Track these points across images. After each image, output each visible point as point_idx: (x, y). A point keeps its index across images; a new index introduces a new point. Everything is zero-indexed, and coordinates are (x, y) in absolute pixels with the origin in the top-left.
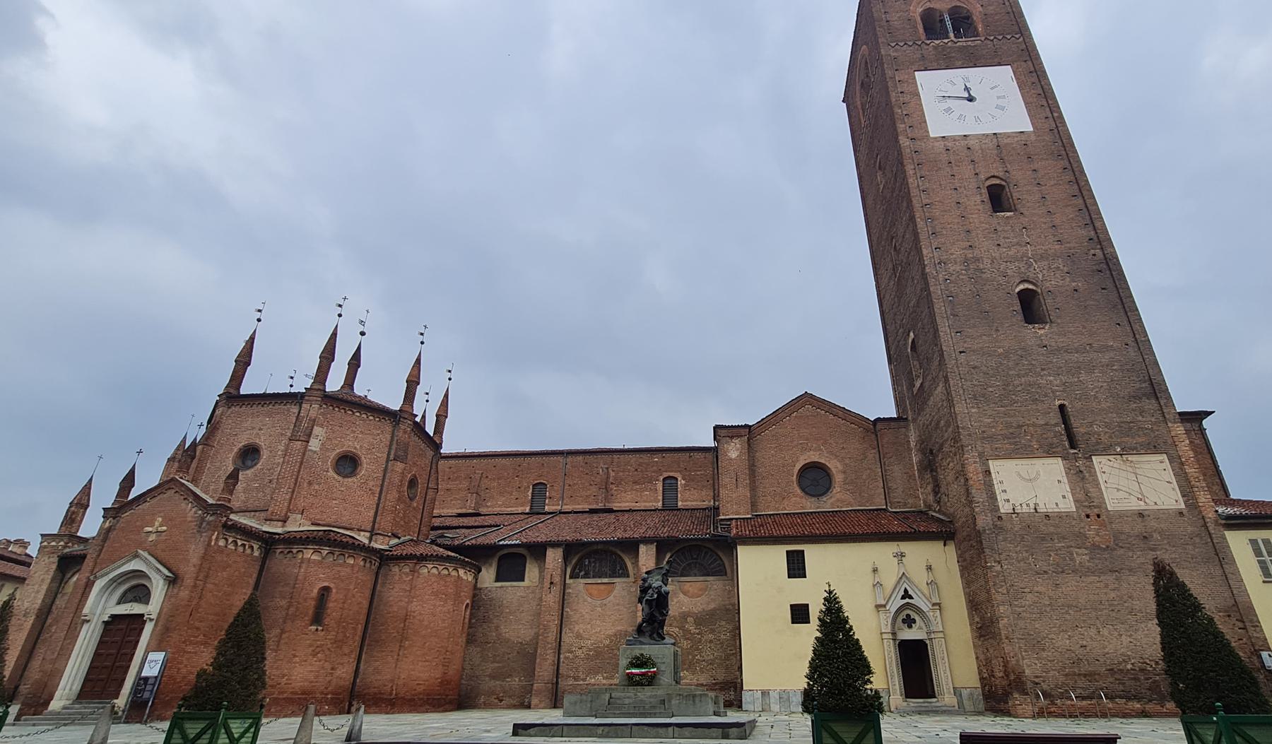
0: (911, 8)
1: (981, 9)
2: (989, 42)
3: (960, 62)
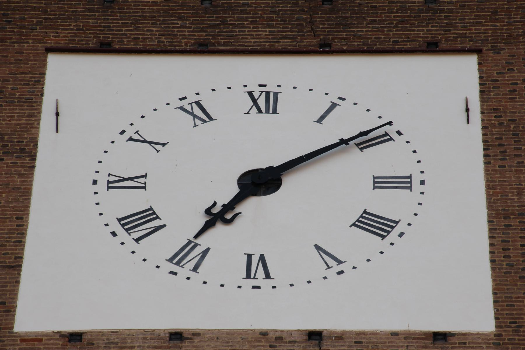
0: (25, 202)
3: (265, 32)
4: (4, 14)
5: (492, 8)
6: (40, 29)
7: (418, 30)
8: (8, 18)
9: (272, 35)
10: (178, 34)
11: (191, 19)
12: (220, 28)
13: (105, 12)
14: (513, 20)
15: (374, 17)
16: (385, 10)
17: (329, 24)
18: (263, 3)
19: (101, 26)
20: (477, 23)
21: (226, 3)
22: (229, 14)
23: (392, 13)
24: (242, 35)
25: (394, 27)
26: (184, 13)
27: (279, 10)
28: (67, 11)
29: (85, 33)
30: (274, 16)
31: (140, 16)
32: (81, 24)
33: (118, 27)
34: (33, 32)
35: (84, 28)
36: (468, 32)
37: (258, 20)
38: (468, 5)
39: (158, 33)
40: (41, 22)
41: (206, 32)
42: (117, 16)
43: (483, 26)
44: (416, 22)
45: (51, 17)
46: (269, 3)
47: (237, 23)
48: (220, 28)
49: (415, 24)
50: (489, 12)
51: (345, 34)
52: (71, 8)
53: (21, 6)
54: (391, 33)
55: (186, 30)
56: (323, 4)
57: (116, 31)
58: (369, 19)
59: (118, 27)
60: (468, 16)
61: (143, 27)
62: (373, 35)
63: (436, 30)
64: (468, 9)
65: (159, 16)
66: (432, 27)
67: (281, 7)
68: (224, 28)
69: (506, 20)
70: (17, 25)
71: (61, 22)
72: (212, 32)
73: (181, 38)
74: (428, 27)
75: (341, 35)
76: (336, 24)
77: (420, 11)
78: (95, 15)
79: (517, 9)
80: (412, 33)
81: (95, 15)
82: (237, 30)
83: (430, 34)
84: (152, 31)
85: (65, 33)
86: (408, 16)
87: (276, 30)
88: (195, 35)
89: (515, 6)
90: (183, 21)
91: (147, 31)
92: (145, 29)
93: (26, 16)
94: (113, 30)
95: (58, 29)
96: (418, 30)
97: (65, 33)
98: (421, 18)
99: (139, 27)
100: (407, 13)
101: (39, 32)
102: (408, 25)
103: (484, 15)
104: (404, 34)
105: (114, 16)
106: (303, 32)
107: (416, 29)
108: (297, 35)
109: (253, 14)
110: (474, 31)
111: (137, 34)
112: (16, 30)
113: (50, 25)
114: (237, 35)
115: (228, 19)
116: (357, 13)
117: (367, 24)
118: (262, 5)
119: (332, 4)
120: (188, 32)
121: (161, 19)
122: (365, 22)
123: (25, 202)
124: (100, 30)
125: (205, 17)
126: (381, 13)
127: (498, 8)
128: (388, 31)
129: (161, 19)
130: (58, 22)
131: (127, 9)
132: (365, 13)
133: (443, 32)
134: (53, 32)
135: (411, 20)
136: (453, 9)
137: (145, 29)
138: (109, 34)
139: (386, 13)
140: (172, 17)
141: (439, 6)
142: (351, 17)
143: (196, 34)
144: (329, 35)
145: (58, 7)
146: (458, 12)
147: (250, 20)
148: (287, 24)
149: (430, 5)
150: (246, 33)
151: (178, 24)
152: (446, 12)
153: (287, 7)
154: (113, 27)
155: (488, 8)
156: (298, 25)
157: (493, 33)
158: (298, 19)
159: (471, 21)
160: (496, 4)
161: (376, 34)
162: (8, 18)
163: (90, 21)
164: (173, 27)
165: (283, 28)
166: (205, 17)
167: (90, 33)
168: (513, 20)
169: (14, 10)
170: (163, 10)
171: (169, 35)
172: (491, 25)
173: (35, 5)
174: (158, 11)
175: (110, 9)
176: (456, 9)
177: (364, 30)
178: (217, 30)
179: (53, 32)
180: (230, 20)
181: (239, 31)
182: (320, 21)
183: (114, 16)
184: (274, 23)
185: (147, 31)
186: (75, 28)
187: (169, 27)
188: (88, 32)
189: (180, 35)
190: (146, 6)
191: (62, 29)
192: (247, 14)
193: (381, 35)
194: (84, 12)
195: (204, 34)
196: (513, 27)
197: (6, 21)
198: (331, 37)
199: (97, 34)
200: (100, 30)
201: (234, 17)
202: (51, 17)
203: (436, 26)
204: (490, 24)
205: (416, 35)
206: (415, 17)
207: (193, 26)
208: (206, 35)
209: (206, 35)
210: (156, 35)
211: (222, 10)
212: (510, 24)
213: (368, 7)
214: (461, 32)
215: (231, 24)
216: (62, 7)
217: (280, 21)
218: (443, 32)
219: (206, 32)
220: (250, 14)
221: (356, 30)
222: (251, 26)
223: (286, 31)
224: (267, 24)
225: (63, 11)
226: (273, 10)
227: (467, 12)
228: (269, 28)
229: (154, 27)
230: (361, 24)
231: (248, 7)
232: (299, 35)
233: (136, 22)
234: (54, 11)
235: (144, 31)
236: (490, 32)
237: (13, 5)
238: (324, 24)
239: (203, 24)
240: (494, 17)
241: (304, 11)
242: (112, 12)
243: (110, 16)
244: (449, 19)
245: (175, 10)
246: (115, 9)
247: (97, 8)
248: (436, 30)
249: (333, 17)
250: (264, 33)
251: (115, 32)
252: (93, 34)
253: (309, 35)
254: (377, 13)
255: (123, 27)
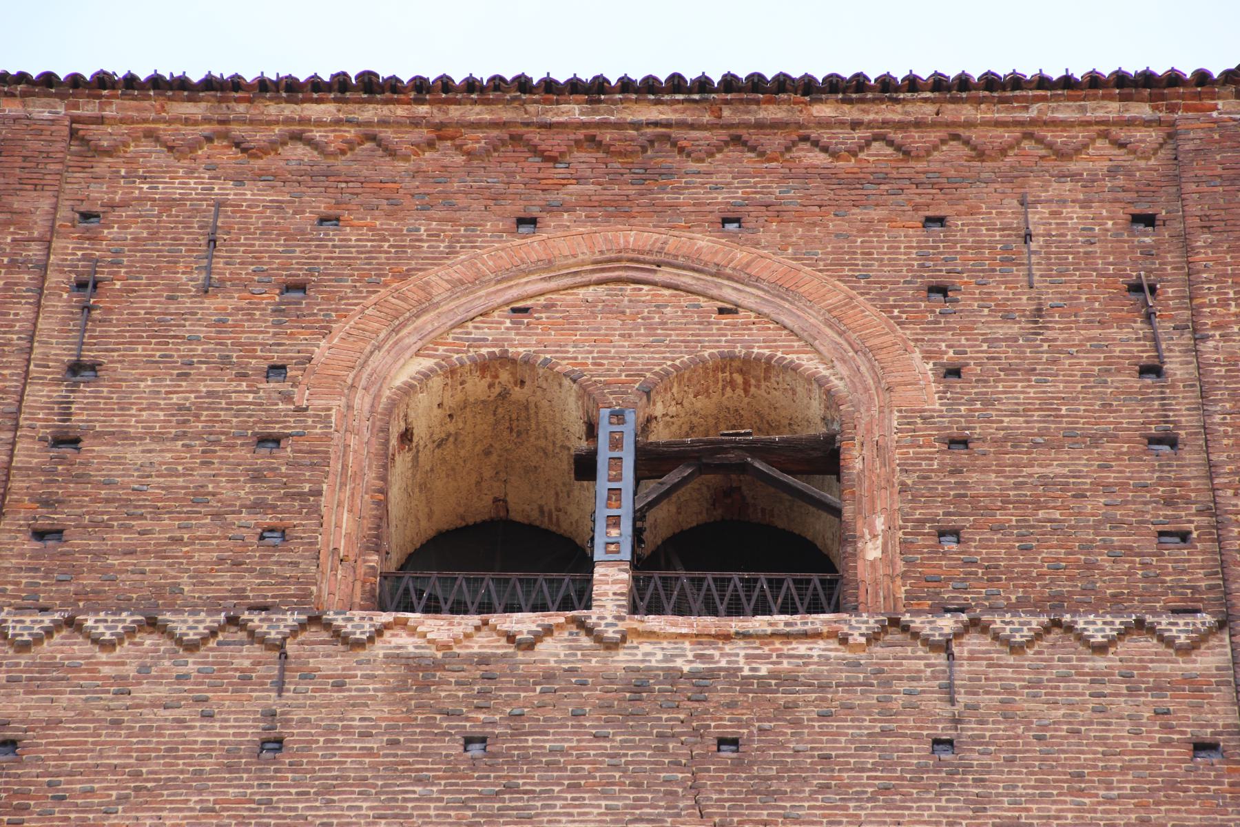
0: (321, 350)
1: (931, 396)
2: (918, 660)
4: (49, 784)
5: (1071, 766)
6: (124, 811)
7: (918, 808)
8: (58, 791)
9: (612, 814)
10: (415, 813)
11: (443, 782)
12: (503, 801)
13: (261, 770)
14: (1116, 792)
15: (826, 778)
16: (849, 763)
17: (732, 792)
18: (593, 748)
19: (253, 801)
20: (1041, 795)
21: (516, 748)
22: (522, 771)
23: (863, 770)
24: (550, 814)
25: (868, 800)
26: (427, 770)
27: (627, 763)
28: (182, 772)
29: (218, 817)
30: (617, 775)
31: (336, 778)
32: (212, 798)
33: (289, 801)
34: (108, 819)
35: (217, 807)
36: (1023, 814)
37: (583, 782)
38: (1021, 759)
39: (371, 813)
40: (127, 797)
41: (473, 808)
42: (286, 778)
43: (1054, 802)
44: (915, 791)
45: (149, 785)
46: (605, 748)
47: (538, 789)
48: (503, 801)
49: (912, 794)
50: (1065, 774)
51: (765, 812)
52: (190, 765)
53: (86, 766)
54: (863, 813)
55: (432, 805)
56: (719, 750)
57: (284, 809)
58: (815, 782)
59: (289, 801)
60: (1022, 781)
61: (341, 801)
62: (824, 816)
63: (957, 809)
64: (1020, 766)
65: (375, 777)
66: (948, 801)
67: (632, 756)
68: (511, 800)
69: (1101, 793)
70: (77, 805)
71: (169, 795)
72: (486, 808)
73: (420, 821)
74: (940, 800)
75: (757, 815)
76: (747, 793)
77: (922, 769)
78: (241, 778)
79: (1124, 769)
80: (907, 812)
81: (241, 778)
82: (539, 804)
83: (945, 816)
84: (360, 808)
85: (177, 817)
86: (897, 778)
87: (620, 804)
88: (449, 816)
89: (1119, 764)
90: (426, 785)
91: (350, 808)
92: (346, 805)
93: (96, 786)
94: (278, 808)
95: (161, 810)
96: (918, 808)
97: (177, 817)
98: (925, 782)
99: (334, 801)
100: (895, 771)
101: (123, 818)
102: (898, 797)
103: (1055, 781)
104: (890, 815)
105: (281, 779)
106: (676, 807)
107: (915, 805)
108: (664, 814)
109: (573, 770)
110: (1035, 813)
111: (329, 816)
112: (73, 816)
113: (146, 802)
114: (538, 815)
115: (521, 781)
116: (790, 770)
117: (813, 793)
118: (592, 752)
119: (737, 751)
120: (436, 808)
121: (380, 783)
122: (807, 789)
123: (321, 350)
124: (251, 810)
125: (473, 777)
126: (840, 771)
127: (1084, 767)
128: (856, 808)
129: (380, 783)
130: (162, 795)
131: (308, 763)
132: (807, 770)
133: (971, 813)
134: (152, 817)
135: (902, 786)
136: (990, 765)
137: (346, 805)
138: (269, 817)
139: (852, 770)
140: (404, 778)
141: (961, 759)
142: (779, 778)
143: (452, 813)
144: (731, 815)
145: (165, 765)
146: (1002, 773)
147: (566, 782)
148: (644, 792)
149: (943, 756)
150: (558, 810)
151: (414, 792)
152: (976, 772)
153: (644, 755)
154: (278, 801)
155: (1063, 766)
156: (667, 793)
157: (1077, 818)
158: (667, 781)
159: (1030, 791)
160: (1079, 759)
161: (830, 815)
162: (58, 791)
163: (231, 790)
164: (405, 800)
165: (634, 799)
166: (473, 777)
167: (229, 817)
168: (1116, 792)
169: (71, 774)
170: (382, 763)
171: (396, 816)
172: (1072, 802)
173: (116, 762)
174: (374, 767)
175: (273, 764)
176: (997, 765)
177: (806, 804)
178: (497, 805)
179: (152, 817)
180: (524, 784)
181: (543, 807)
182: (714, 785)
183: (281, 779)
184: (617, 788)
185: (350, 808)
186: (198, 807)
187: (396, 800)
188: (225, 814)
189: (419, 816)
190: (347, 756)
191: (171, 810)
192: (560, 770)
193: (842, 815)
194: (217, 772)
195: (470, 813)
196: (1117, 808)
197: (53, 797)
198: (736, 819)
199: (244, 817)
200: (251, 810)
201: (533, 778)
202: (149, 785)
203: (957, 801)
204: (1068, 799)
205: (915, 818)
206: (911, 780)
207: (446, 797)
208: (474, 816)
209: (474, 816)
210: (368, 816)
211: (507, 763)
212: (1110, 800)
213: (812, 757)
214: (1009, 814)
215: (526, 792)
216: (172, 765)
217: (630, 785)
218: (971, 813)
219: (473, 808)
220: (566, 770)
221: (788, 805)
222: (569, 796)
223: (641, 807)
224: (602, 792)
225: (173, 773)
226: (615, 761)
227: (1019, 773)
228: (606, 798)
229: (365, 800)
230: (799, 792)
231: (562, 756)
232: (670, 815)
233: (327, 790)
234: (155, 773)
235: (342, 809)
236: (1070, 815)
237: (70, 763)
238: (722, 792)
239: (466, 792)
240: (1076, 785)
241: (679, 764)
242: (276, 771)
243: (272, 778)
244: (984, 787)
245: (409, 764)
246: (284, 763)
247: (246, 764)
248: (957, 809)
249: (740, 777)
250: (596, 811)
251: (281, 813)
252: (234, 817)
253: (690, 815)
254: (833, 770)
255: (298, 801)
